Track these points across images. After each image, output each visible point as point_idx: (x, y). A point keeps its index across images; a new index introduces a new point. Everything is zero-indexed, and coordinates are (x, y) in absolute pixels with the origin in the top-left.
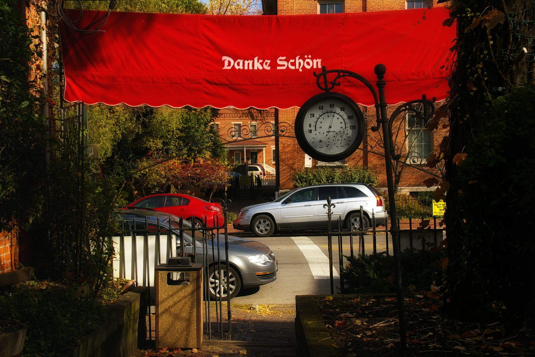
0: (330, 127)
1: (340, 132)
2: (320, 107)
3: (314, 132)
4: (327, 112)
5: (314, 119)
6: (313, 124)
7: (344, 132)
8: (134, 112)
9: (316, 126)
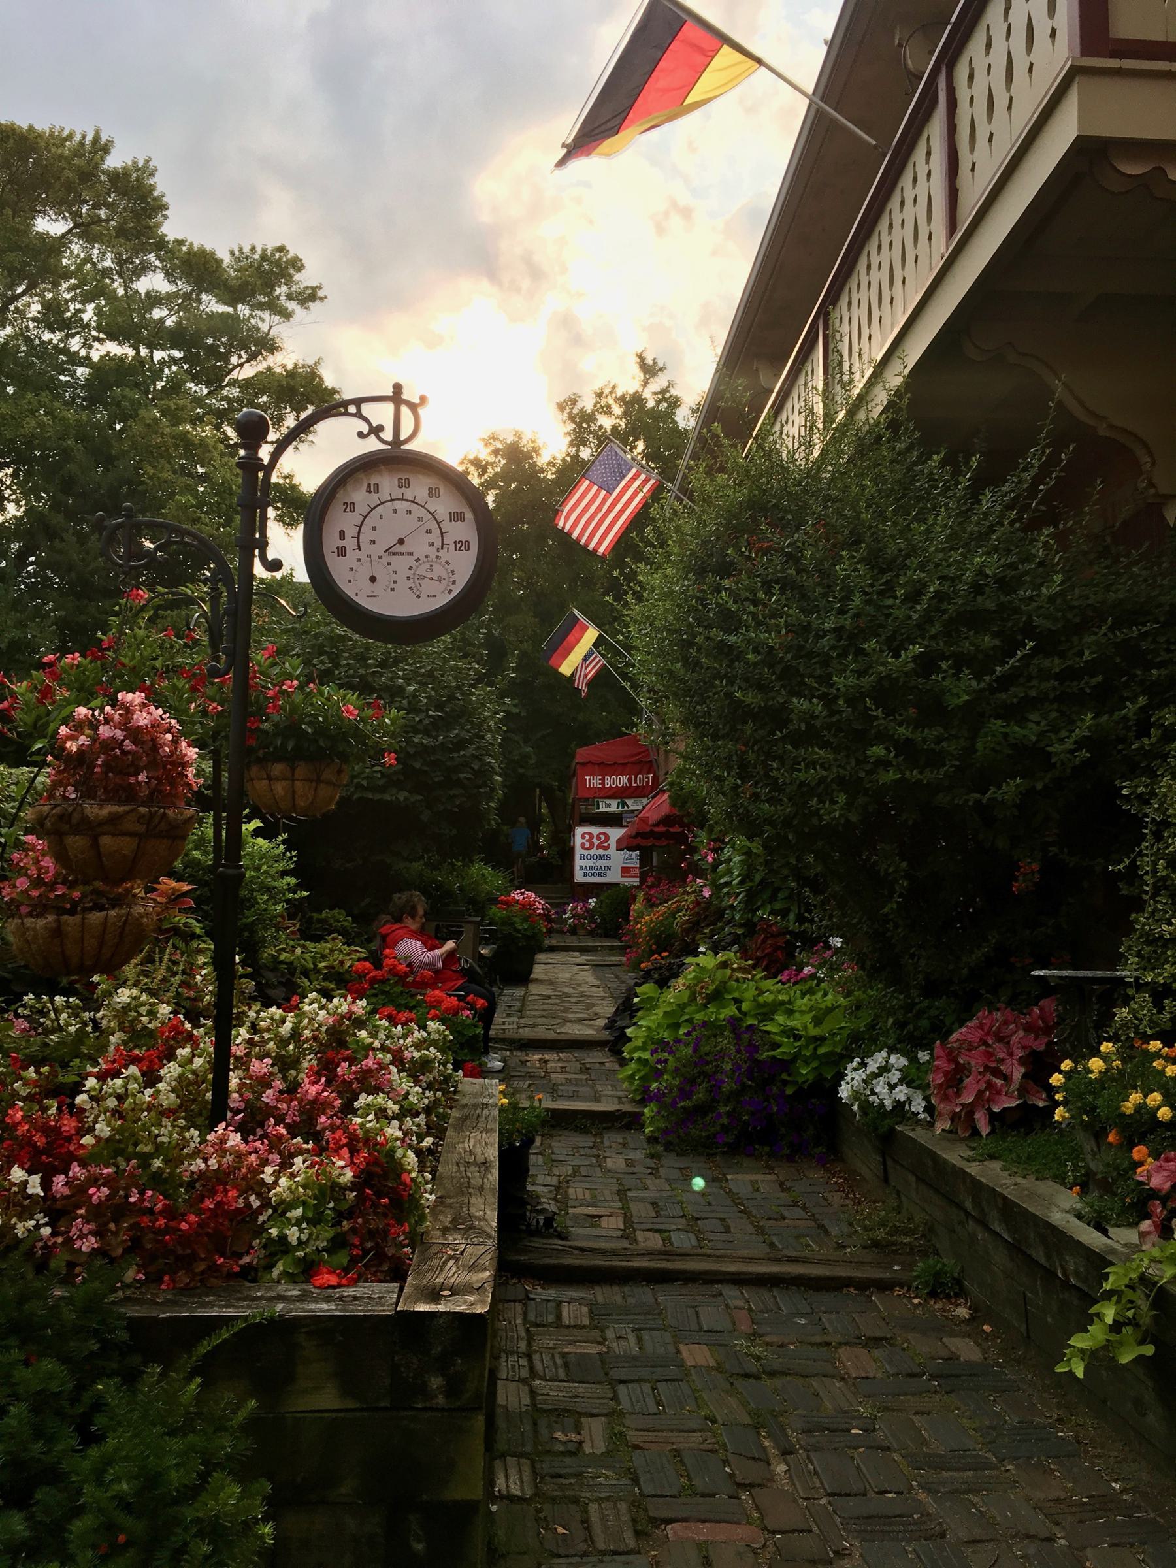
0: (401, 541)
1: (427, 556)
2: (369, 485)
3: (352, 554)
4: (392, 500)
5: (355, 518)
6: (351, 532)
7: (438, 557)
8: (1009, 1004)
9: (358, 538)
